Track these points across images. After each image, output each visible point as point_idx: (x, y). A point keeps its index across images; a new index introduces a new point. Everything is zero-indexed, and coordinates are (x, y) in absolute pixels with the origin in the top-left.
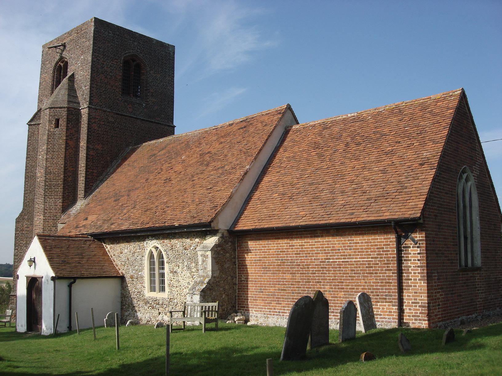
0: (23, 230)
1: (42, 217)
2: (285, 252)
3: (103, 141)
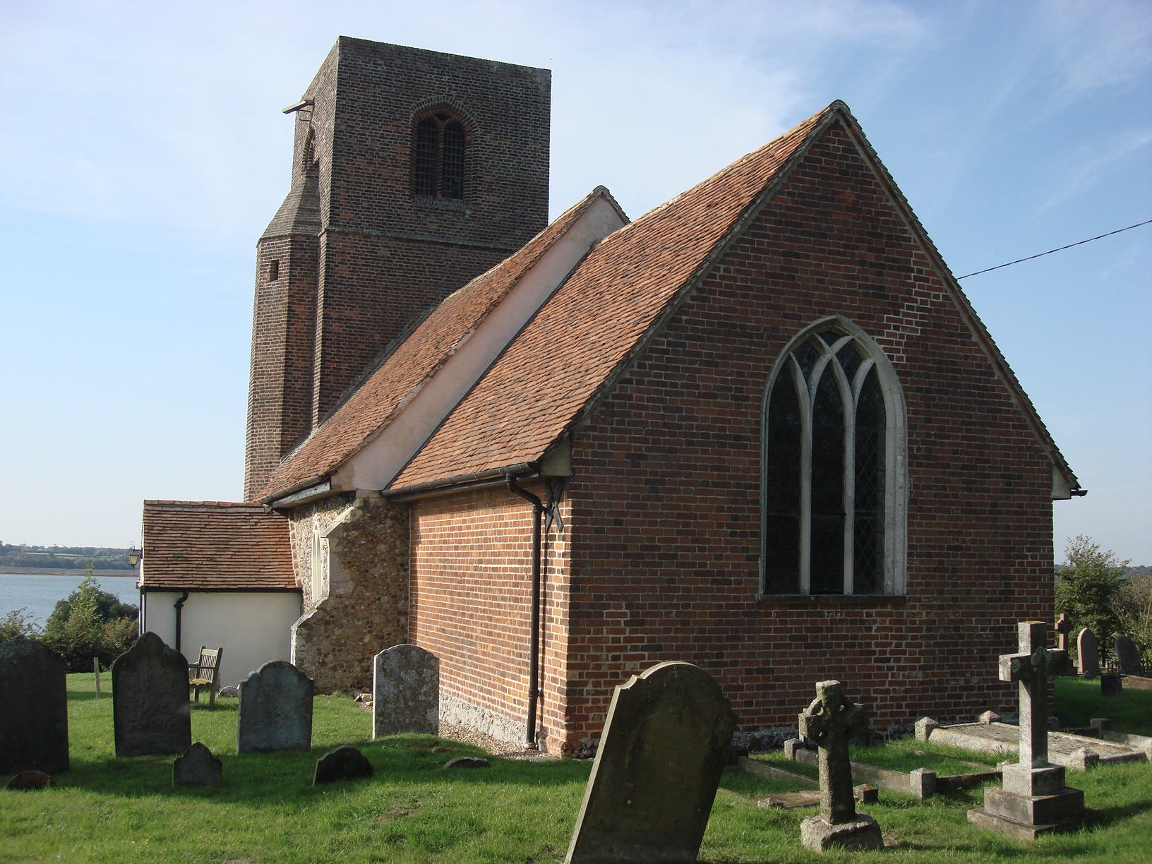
3: (364, 300)
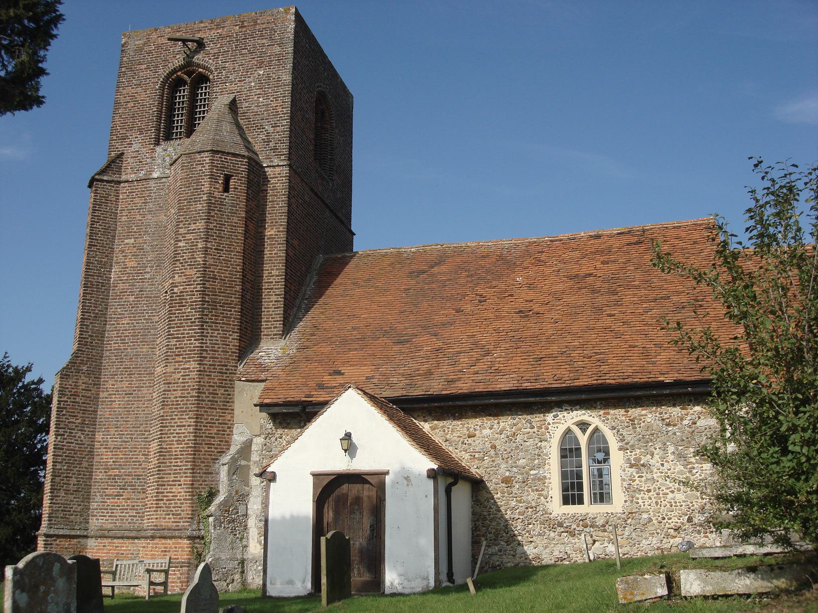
0: (76, 395)
1: (193, 365)
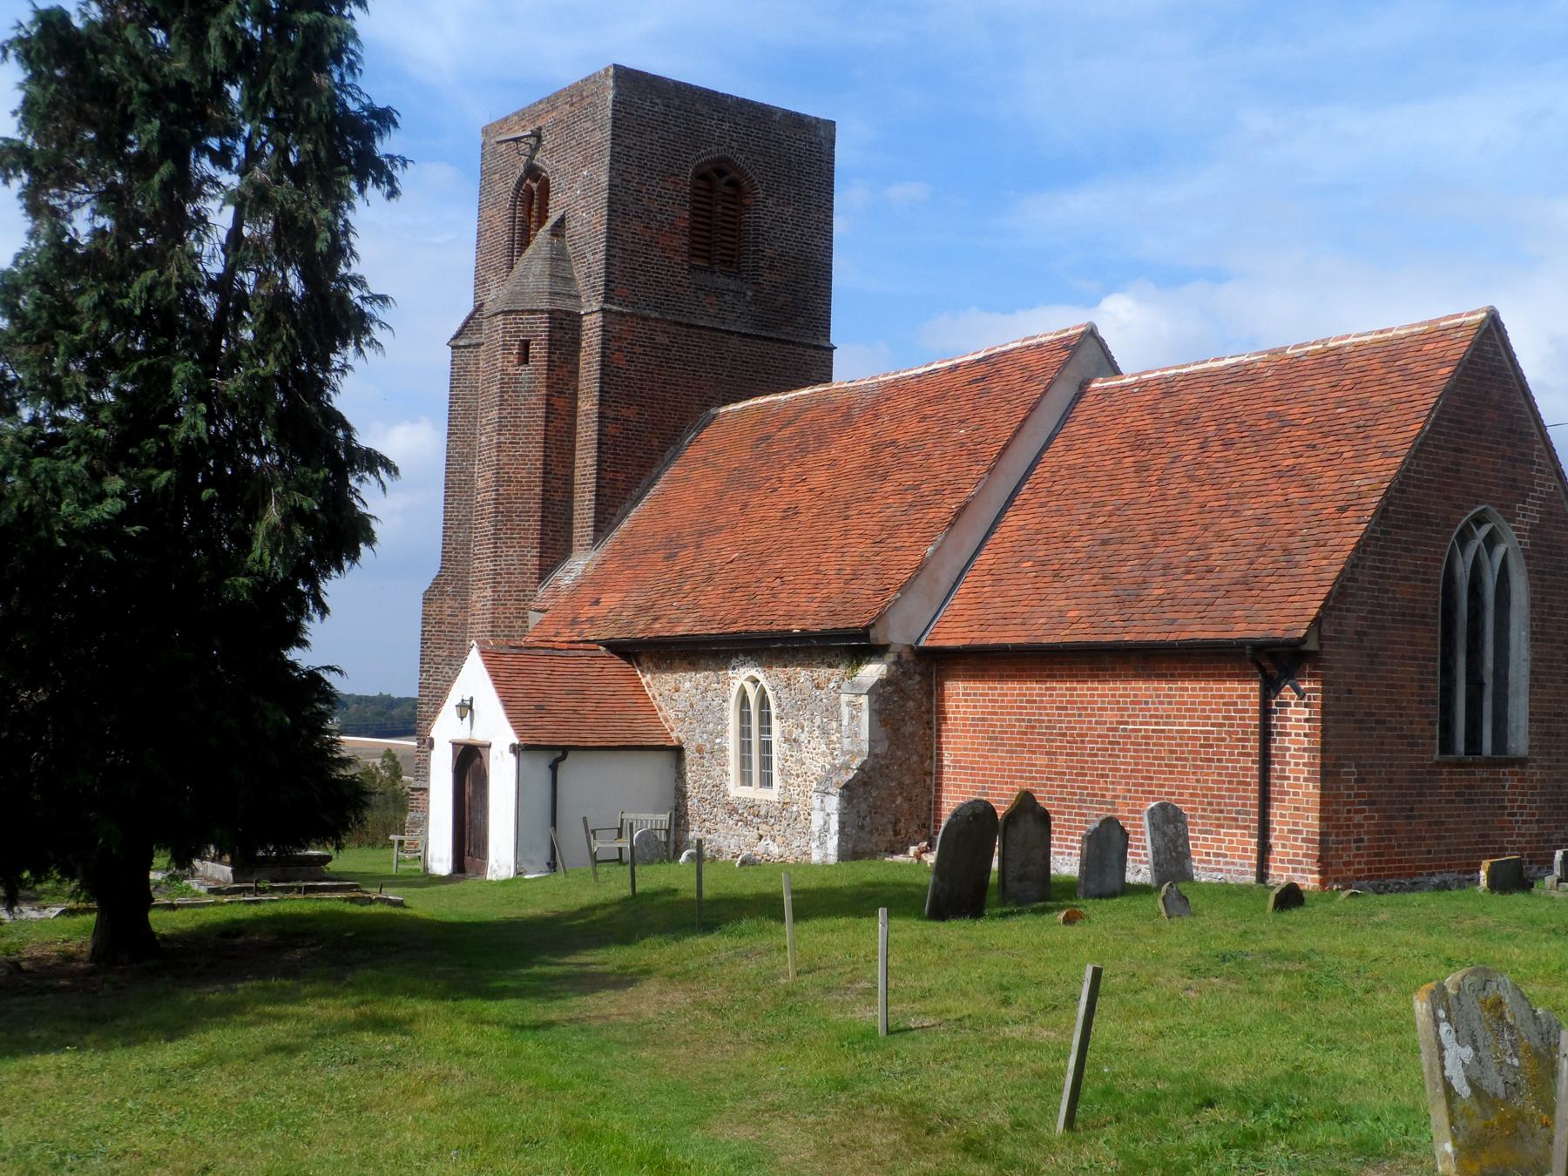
1: (488, 592)
2: (1035, 702)
